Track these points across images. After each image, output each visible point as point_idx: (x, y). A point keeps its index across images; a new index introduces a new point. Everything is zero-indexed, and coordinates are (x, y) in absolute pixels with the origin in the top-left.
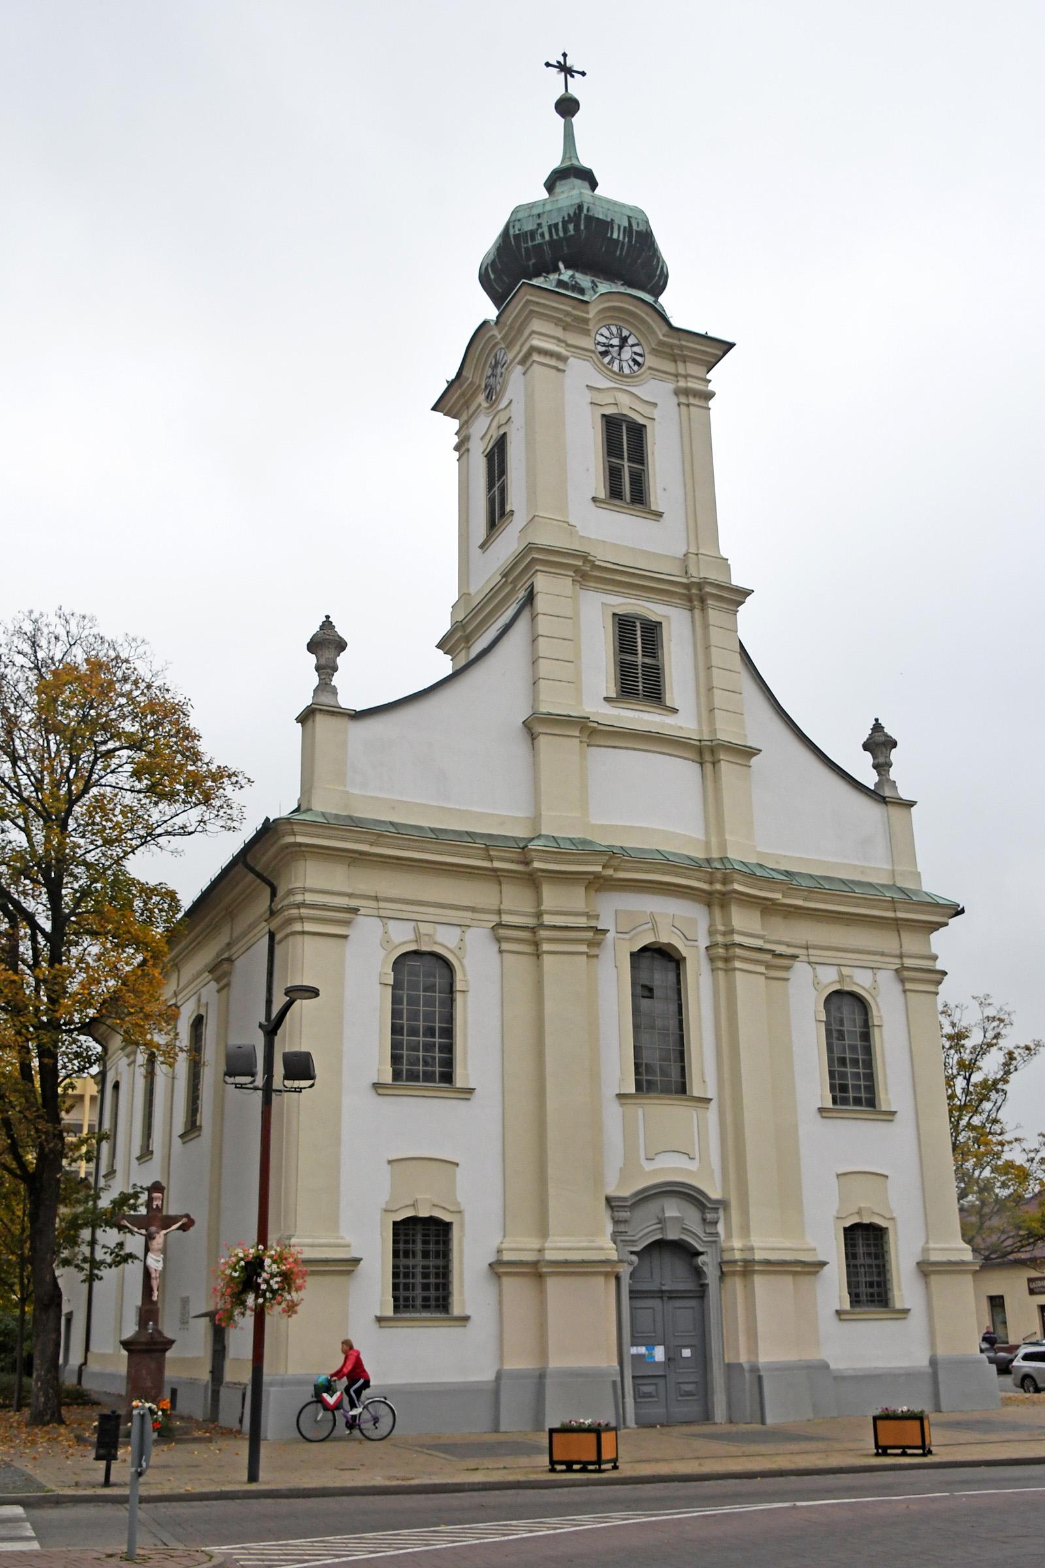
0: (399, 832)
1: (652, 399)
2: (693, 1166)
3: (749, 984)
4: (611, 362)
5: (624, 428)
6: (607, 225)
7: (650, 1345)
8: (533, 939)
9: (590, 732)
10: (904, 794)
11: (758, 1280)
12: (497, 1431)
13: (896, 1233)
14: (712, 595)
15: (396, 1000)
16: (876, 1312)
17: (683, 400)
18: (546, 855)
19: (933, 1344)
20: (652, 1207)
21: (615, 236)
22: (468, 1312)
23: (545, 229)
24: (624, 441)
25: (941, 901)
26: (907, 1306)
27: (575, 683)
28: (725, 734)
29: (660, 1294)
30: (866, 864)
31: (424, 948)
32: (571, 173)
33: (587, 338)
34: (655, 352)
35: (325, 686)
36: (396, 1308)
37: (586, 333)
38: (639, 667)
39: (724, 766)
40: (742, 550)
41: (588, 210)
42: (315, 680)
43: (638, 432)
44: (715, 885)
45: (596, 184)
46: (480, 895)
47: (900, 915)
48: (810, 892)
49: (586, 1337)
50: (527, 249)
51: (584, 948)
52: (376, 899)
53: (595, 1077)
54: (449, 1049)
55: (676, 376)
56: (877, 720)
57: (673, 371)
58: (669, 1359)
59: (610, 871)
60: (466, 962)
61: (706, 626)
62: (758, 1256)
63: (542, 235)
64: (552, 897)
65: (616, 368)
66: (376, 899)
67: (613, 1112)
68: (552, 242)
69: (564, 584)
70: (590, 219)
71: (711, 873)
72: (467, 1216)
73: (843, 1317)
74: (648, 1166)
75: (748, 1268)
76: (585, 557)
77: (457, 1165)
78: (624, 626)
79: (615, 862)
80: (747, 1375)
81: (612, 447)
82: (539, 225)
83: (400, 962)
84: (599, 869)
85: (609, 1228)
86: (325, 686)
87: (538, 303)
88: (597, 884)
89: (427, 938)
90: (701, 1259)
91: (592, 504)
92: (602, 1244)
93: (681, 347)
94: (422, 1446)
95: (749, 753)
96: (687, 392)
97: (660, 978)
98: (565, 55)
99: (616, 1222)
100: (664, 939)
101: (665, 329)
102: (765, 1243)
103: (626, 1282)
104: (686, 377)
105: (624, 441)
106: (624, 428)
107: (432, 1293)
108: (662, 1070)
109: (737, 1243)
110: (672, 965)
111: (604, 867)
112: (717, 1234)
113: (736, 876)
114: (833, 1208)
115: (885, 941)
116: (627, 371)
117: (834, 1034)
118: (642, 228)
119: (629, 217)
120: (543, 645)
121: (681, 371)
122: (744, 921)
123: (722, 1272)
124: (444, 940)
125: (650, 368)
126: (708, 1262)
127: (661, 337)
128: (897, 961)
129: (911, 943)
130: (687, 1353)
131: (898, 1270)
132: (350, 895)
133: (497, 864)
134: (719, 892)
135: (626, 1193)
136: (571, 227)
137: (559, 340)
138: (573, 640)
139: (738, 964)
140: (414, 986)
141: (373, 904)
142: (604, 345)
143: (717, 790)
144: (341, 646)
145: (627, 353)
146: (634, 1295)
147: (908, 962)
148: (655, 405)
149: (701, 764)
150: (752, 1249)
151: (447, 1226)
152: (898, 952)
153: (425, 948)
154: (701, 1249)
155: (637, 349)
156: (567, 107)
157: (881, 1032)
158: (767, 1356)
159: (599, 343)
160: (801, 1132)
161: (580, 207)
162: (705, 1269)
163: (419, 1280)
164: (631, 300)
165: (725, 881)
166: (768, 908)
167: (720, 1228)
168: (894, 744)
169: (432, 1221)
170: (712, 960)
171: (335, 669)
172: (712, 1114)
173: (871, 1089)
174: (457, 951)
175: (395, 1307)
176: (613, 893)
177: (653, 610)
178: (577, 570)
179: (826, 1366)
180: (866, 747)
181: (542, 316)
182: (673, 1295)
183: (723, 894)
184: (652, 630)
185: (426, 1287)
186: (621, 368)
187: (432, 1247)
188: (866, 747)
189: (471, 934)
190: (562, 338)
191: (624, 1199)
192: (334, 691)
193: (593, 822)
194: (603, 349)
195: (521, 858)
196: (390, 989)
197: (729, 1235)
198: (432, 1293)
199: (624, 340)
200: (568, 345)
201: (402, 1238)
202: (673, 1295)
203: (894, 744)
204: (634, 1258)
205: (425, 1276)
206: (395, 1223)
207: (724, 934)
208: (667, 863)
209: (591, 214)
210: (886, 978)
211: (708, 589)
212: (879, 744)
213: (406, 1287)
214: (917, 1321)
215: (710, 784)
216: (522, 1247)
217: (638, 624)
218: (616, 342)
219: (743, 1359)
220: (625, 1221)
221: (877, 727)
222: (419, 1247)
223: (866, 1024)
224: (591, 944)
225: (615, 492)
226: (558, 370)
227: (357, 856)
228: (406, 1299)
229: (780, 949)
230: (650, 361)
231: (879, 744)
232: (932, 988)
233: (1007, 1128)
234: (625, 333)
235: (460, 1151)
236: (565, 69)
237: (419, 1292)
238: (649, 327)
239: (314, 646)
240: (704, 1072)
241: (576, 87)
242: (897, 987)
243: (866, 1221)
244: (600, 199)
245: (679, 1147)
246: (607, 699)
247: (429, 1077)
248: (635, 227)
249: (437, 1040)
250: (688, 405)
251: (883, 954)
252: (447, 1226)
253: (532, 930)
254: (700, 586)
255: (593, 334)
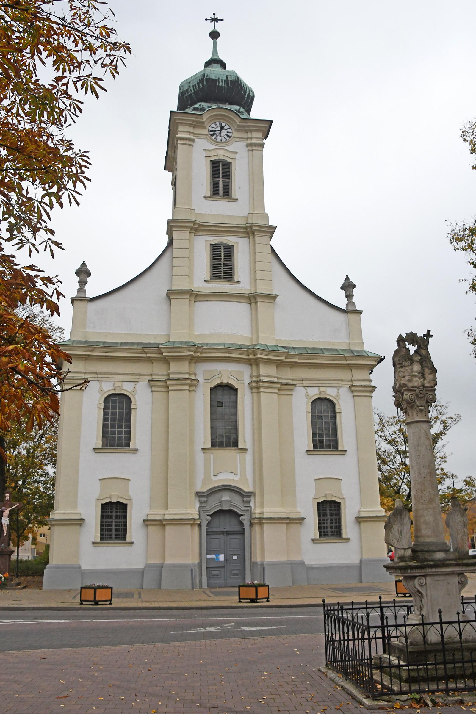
0: (105, 346)
1: (236, 151)
2: (237, 478)
3: (269, 399)
4: (216, 138)
5: (221, 165)
6: (216, 81)
7: (218, 554)
8: (164, 385)
9: (195, 296)
10: (358, 308)
11: (266, 526)
12: (361, 582)
13: (345, 505)
14: (259, 230)
15: (105, 414)
16: (335, 539)
17: (250, 148)
18: (169, 349)
19: (362, 554)
20: (217, 496)
21: (220, 85)
22: (133, 540)
23: (192, 88)
24: (220, 171)
25: (370, 354)
26: (349, 537)
27: (190, 276)
28: (262, 289)
29: (222, 533)
30: (336, 341)
31: (117, 392)
32: (215, 61)
33: (205, 130)
34: (237, 130)
35: (82, 289)
36: (320, 535)
37: (204, 127)
38: (222, 264)
39: (259, 304)
40: (275, 211)
41: (207, 76)
42: (78, 286)
43: (227, 166)
44: (250, 356)
45: (225, 65)
46: (144, 368)
47: (349, 362)
48: (301, 356)
49: (185, 549)
50: (186, 97)
51: (187, 387)
52: (96, 373)
53: (192, 442)
54: (336, 436)
55: (247, 138)
56: (347, 276)
57: (246, 137)
58: (226, 560)
59: (198, 354)
60: (340, 401)
61: (254, 244)
62: (266, 516)
63: (191, 90)
64: (174, 367)
65: (218, 140)
66: (96, 373)
67: (200, 456)
68: (195, 92)
69: (186, 235)
70: (208, 80)
71: (247, 351)
72: (134, 501)
73: (315, 542)
74: (214, 479)
75: (261, 521)
76: (194, 222)
77: (130, 480)
78: (215, 249)
79: (199, 350)
80: (259, 567)
81: (214, 173)
82: (189, 86)
83: (107, 399)
84: (192, 353)
85: (198, 505)
86: (82, 289)
87: (179, 119)
88: (194, 360)
89: (118, 388)
90: (241, 518)
91: (204, 199)
92: (193, 512)
93: (249, 126)
94: (331, 589)
95: (273, 297)
96: (251, 145)
97: (226, 398)
98: (214, 14)
99: (201, 502)
100: (225, 381)
101: (239, 119)
102: (270, 509)
103: (204, 527)
104: (251, 138)
105: (220, 171)
106: (221, 165)
107: (334, 530)
108: (225, 437)
109: (257, 511)
110: (232, 391)
111: (195, 352)
112: (250, 507)
113: (258, 351)
114: (312, 493)
115: (345, 375)
116: (223, 140)
117: (316, 417)
118: (233, 79)
119: (227, 76)
120: (176, 262)
121: (250, 136)
122: (267, 372)
123: (251, 523)
124: (127, 388)
125: (234, 137)
126: (245, 519)
127: (238, 123)
128: (350, 383)
129: (359, 375)
130: (235, 557)
131: (345, 522)
132: (85, 373)
133: (148, 355)
134: (253, 359)
135: (204, 490)
136: (201, 84)
137: (190, 132)
138: (190, 258)
139: (262, 390)
140: (114, 408)
141: (301, 382)
142: (213, 131)
143: (256, 315)
144: (89, 274)
145: (224, 133)
146: (208, 533)
147: (355, 383)
148: (236, 153)
149: (251, 304)
150: (263, 513)
151: (339, 504)
152: (350, 379)
153: (323, 397)
154: (241, 513)
155: (230, 130)
156: (214, 35)
157: (340, 415)
158: (268, 559)
159: (210, 131)
160: (296, 461)
161: (204, 75)
162: (243, 522)
163: (329, 525)
164: (223, 110)
165: (254, 354)
166: (280, 364)
167: (252, 504)
168: (354, 286)
169: (118, 503)
170: (251, 388)
171: (86, 283)
172: (249, 456)
173: (336, 441)
174: (337, 398)
175: (320, 535)
176: (206, 363)
177: (229, 240)
178: (192, 228)
179: (303, 563)
180: (342, 288)
181: (182, 124)
182: (228, 533)
183: (256, 359)
184: (229, 249)
185: (332, 527)
186: (221, 140)
187: (333, 512)
188: (342, 288)
189: (138, 385)
190: (192, 131)
191: (204, 493)
192: (85, 292)
193: (196, 333)
194: (213, 133)
195: (159, 352)
196: (310, 414)
197: (255, 507)
198: (334, 530)
199: (222, 128)
200: (194, 134)
201: (321, 509)
202: (228, 533)
203: (354, 286)
204: (209, 518)
205: (331, 523)
206: (102, 504)
207: (257, 377)
208: (224, 348)
209: (208, 77)
210: (344, 392)
211: (254, 228)
212: (348, 287)
213: (324, 528)
214: (354, 544)
215: (253, 312)
216: (158, 513)
217: (222, 247)
218: (219, 129)
219: (259, 560)
220: (205, 502)
221: (347, 279)
222: (328, 512)
223: (334, 412)
224: (190, 386)
225: (215, 192)
226: (189, 145)
227: (87, 357)
228: (324, 532)
229: (284, 382)
230: (235, 134)
231: (348, 287)
232: (368, 394)
233: (447, 455)
234: (223, 124)
235: (133, 475)
236: (214, 20)
237: (329, 530)
238: (233, 120)
239: (78, 273)
240: (245, 436)
241: (219, 27)
242: (350, 395)
243: (329, 499)
244: (229, 72)
245: (234, 470)
246: (206, 281)
247: (119, 445)
248: (229, 79)
249: (124, 429)
250: (252, 150)
251: (342, 381)
252: (339, 504)
253: (165, 381)
254: (251, 227)
255: (207, 127)
